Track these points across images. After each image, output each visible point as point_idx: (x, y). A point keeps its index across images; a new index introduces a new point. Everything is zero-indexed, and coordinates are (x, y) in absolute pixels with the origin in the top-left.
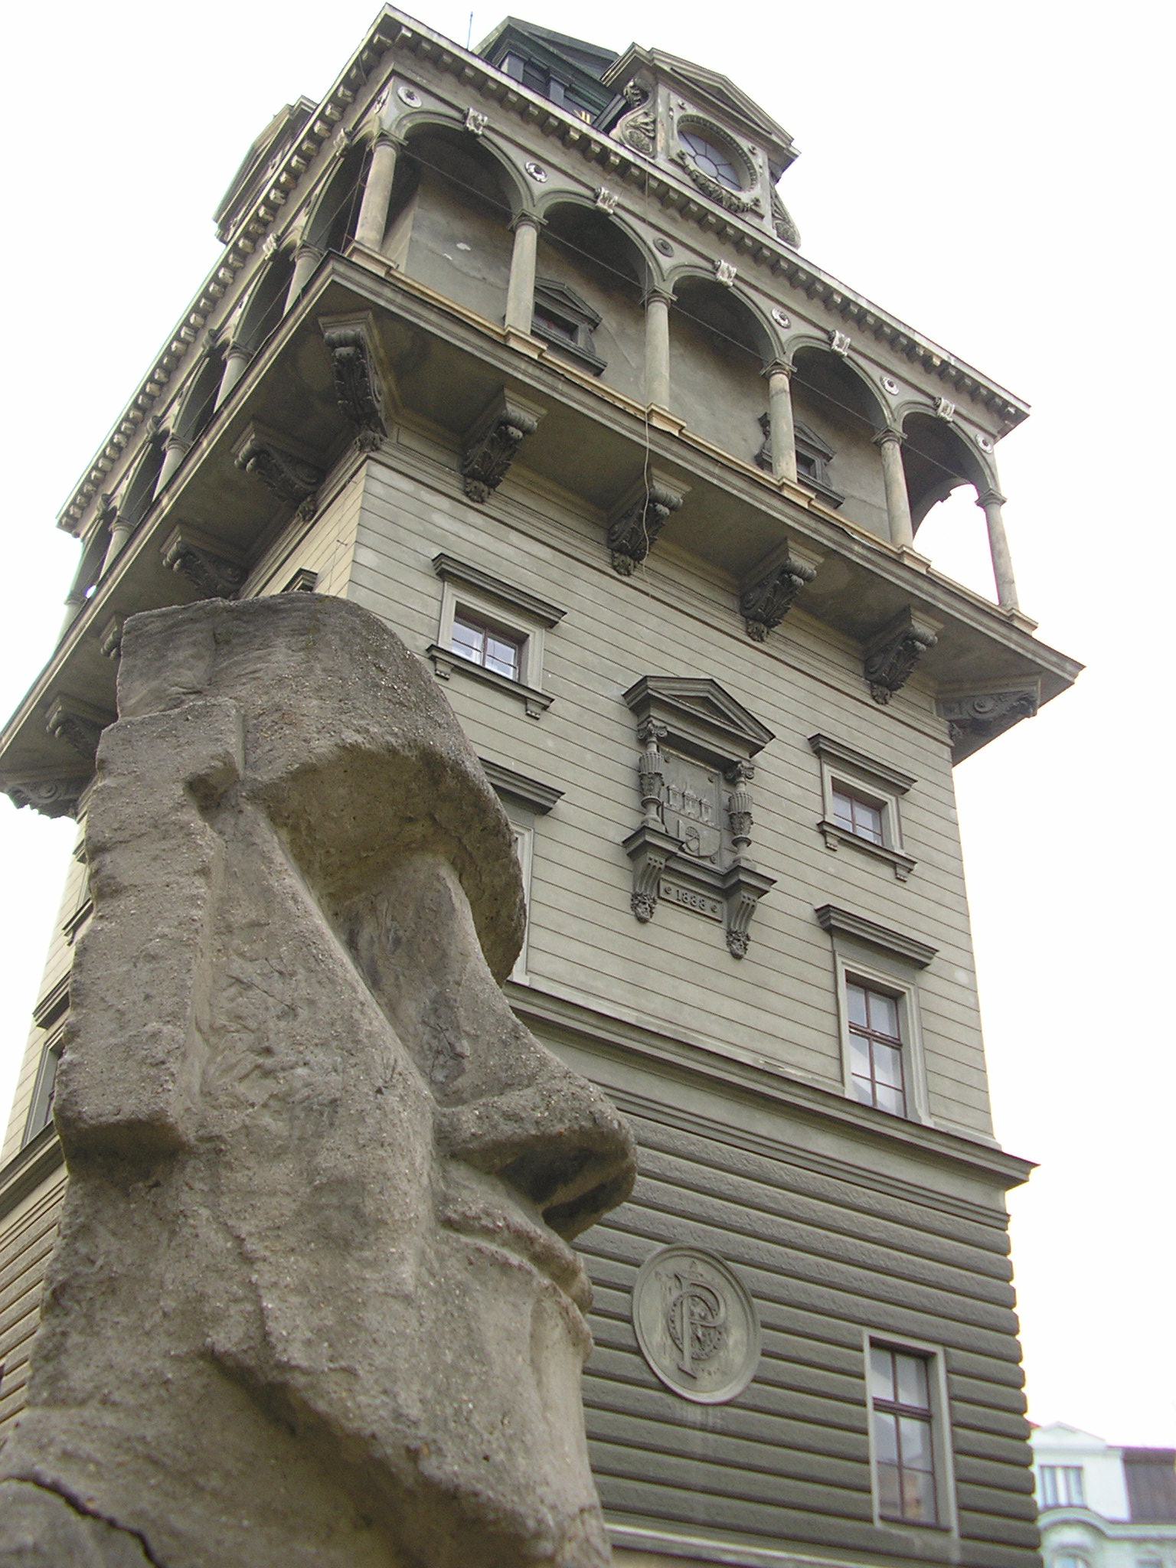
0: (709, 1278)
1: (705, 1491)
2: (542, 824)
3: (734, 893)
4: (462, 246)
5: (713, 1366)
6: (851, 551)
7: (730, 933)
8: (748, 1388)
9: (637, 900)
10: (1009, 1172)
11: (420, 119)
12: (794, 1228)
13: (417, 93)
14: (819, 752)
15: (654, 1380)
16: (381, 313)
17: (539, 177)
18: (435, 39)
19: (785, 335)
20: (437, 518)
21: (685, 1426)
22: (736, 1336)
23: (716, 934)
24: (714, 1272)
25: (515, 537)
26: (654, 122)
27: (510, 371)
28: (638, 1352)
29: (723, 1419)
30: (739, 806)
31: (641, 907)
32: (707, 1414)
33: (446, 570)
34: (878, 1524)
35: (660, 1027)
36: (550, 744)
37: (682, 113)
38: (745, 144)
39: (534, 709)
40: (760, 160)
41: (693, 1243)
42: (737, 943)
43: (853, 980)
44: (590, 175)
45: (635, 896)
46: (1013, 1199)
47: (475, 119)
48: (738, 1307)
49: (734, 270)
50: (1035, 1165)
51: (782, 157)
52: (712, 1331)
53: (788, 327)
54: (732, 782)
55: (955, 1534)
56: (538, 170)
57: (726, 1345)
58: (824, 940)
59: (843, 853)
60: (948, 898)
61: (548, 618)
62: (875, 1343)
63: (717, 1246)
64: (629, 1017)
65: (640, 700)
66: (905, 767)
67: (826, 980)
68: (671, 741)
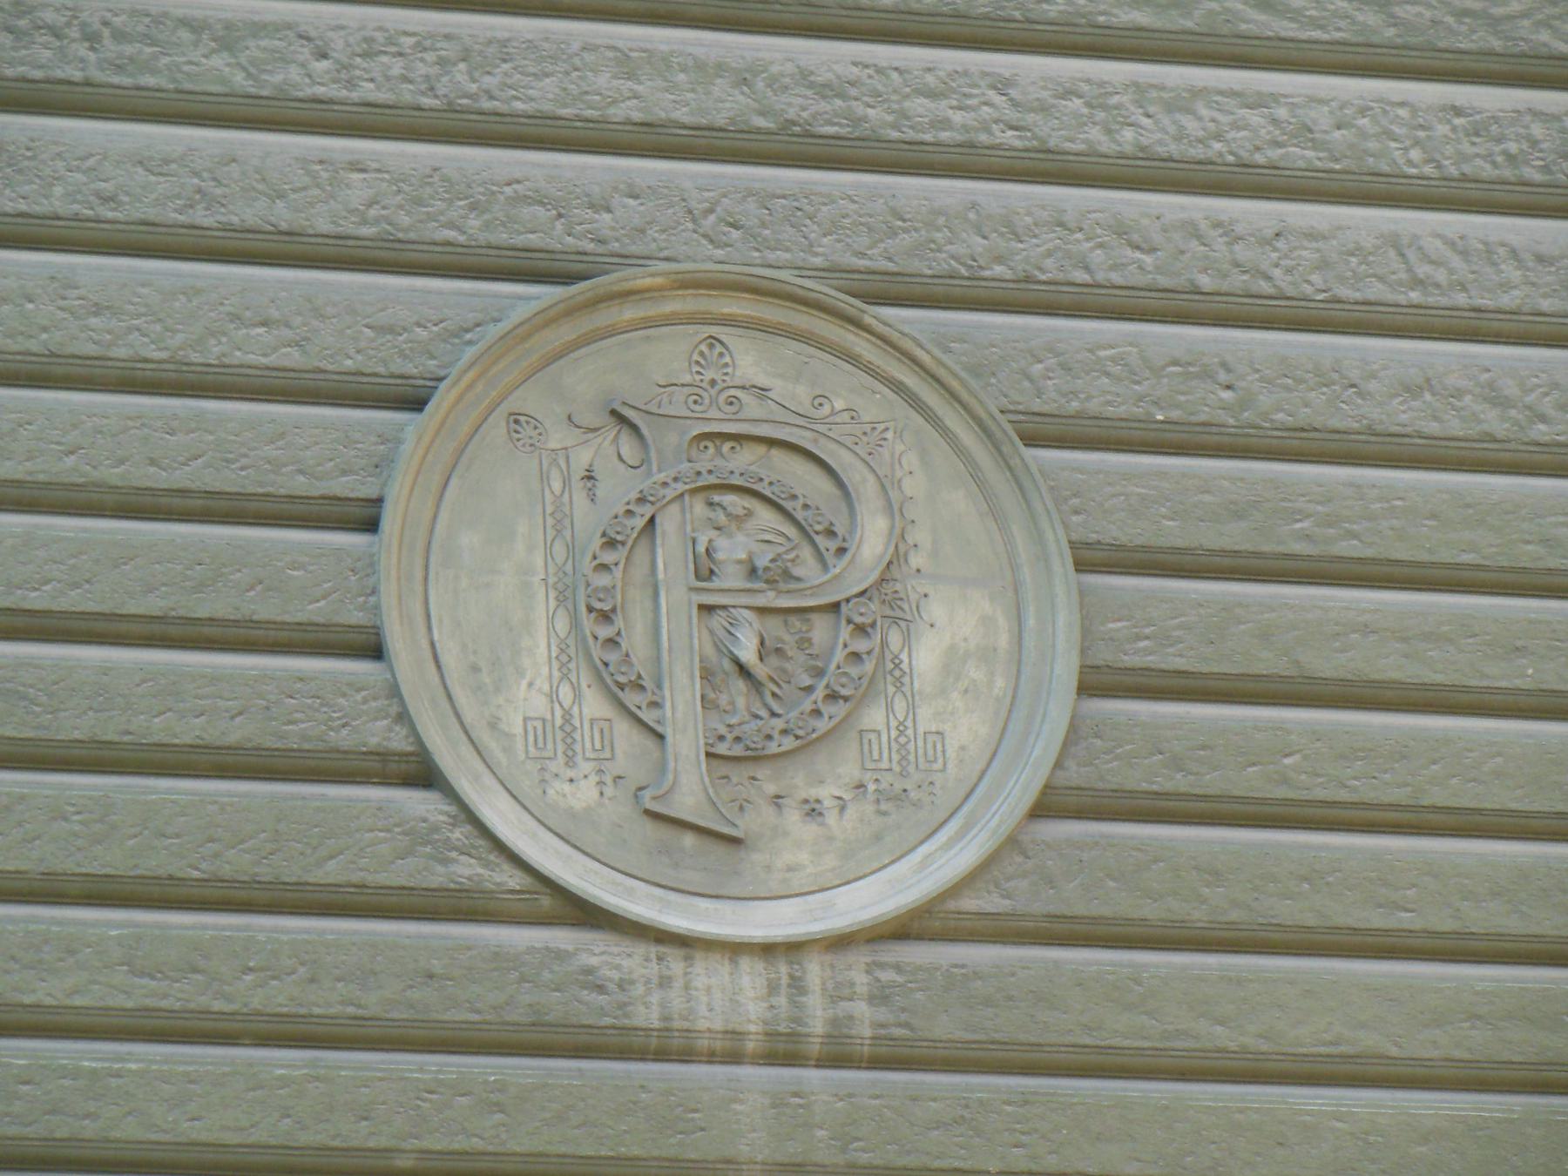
0: (801, 395)
8: (1012, 842)
12: (1260, 101)
15: (512, 879)
21: (686, 1056)
22: (948, 631)
24: (821, 362)
28: (423, 774)
29: (880, 996)
32: (798, 986)
41: (705, 259)
48: (959, 501)
52: (820, 630)
57: (899, 675)
60: (370, 828)
63: (828, 250)
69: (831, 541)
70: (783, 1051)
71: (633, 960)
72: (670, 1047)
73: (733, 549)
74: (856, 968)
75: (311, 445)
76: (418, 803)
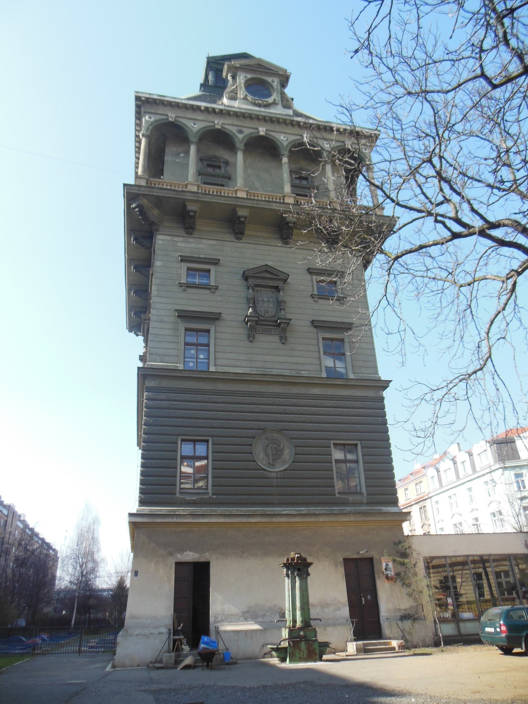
1: (278, 495)
2: (217, 323)
3: (279, 326)
4: (182, 155)
5: (280, 461)
6: (154, 192)
7: (280, 337)
9: (249, 336)
10: (385, 385)
11: (154, 124)
13: (197, 122)
14: (310, 273)
16: (144, 195)
17: (195, 126)
18: (152, 97)
19: (285, 144)
20: (179, 244)
22: (287, 451)
23: (276, 339)
25: (204, 241)
26: (237, 87)
27: (184, 197)
28: (255, 461)
30: (280, 299)
31: (251, 337)
33: (184, 259)
34: (337, 495)
35: (258, 371)
36: (219, 299)
37: (246, 79)
38: (269, 79)
39: (213, 290)
40: (275, 82)
42: (283, 339)
43: (324, 339)
44: (211, 118)
45: (248, 335)
46: (385, 393)
47: (171, 117)
49: (264, 129)
50: (391, 381)
51: (284, 79)
53: (284, 138)
54: (279, 292)
55: (365, 494)
56: (195, 124)
58: (314, 330)
59: (321, 301)
61: (216, 262)
62: (334, 444)
64: (247, 371)
65: (246, 277)
66: (213, 254)
67: (315, 342)
68: (256, 286)
69: (279, 446)
70: (277, 478)
71: (268, 473)
72: (270, 478)
73: (273, 447)
74: (281, 473)
75: (248, 440)
76: (254, 463)
